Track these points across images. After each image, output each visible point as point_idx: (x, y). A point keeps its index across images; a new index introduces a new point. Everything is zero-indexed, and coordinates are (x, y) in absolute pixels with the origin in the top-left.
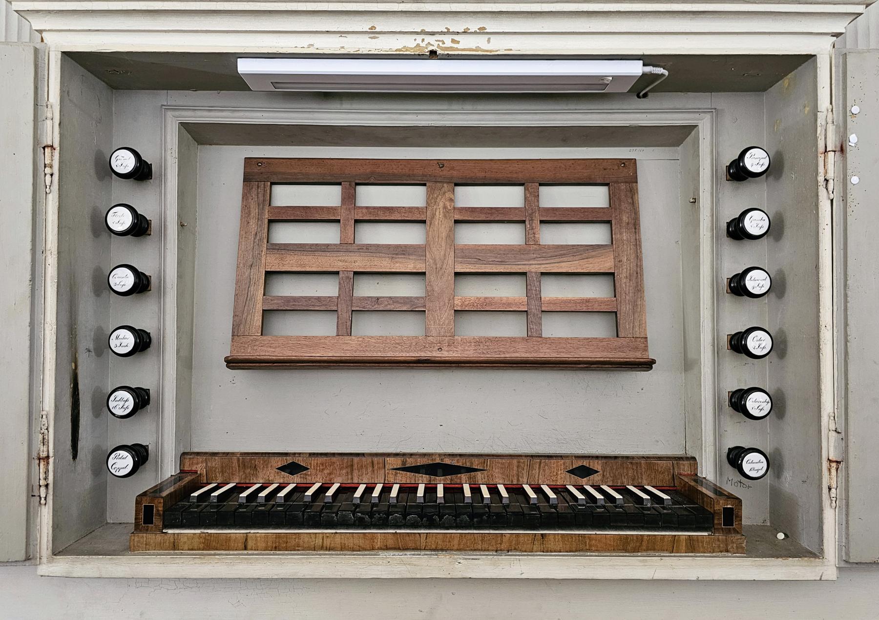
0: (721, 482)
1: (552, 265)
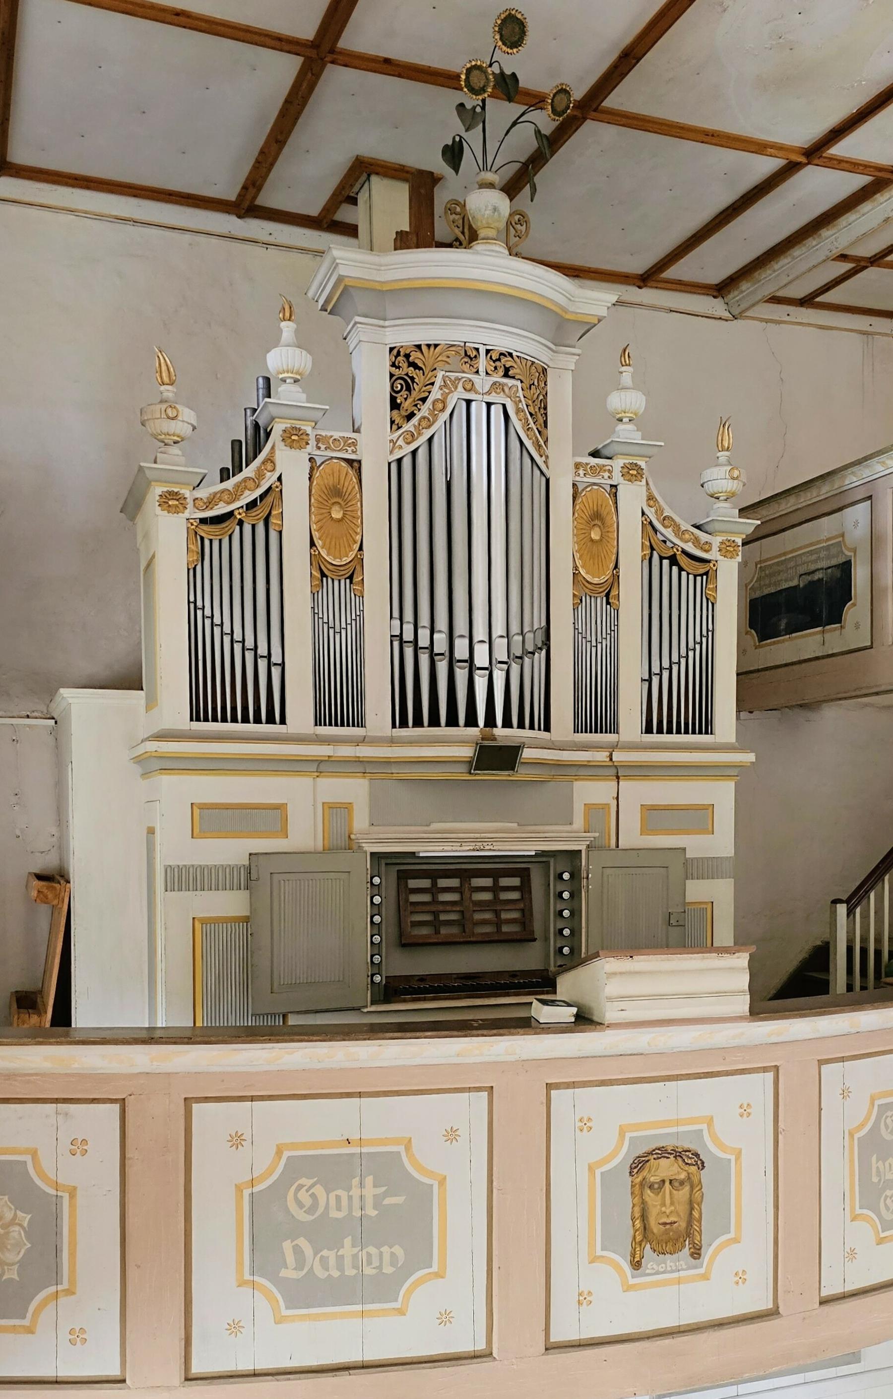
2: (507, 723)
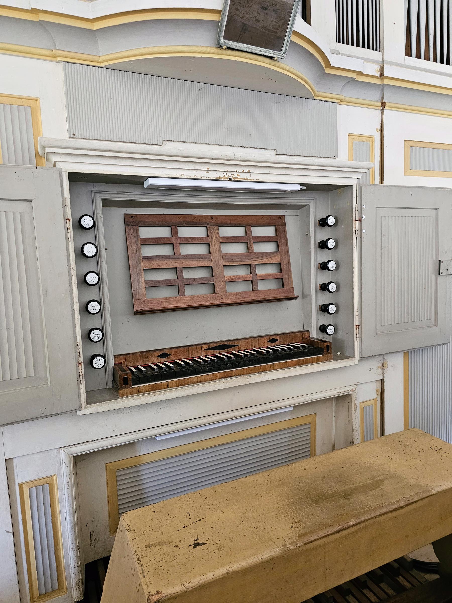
0: (318, 337)
1: (259, 261)
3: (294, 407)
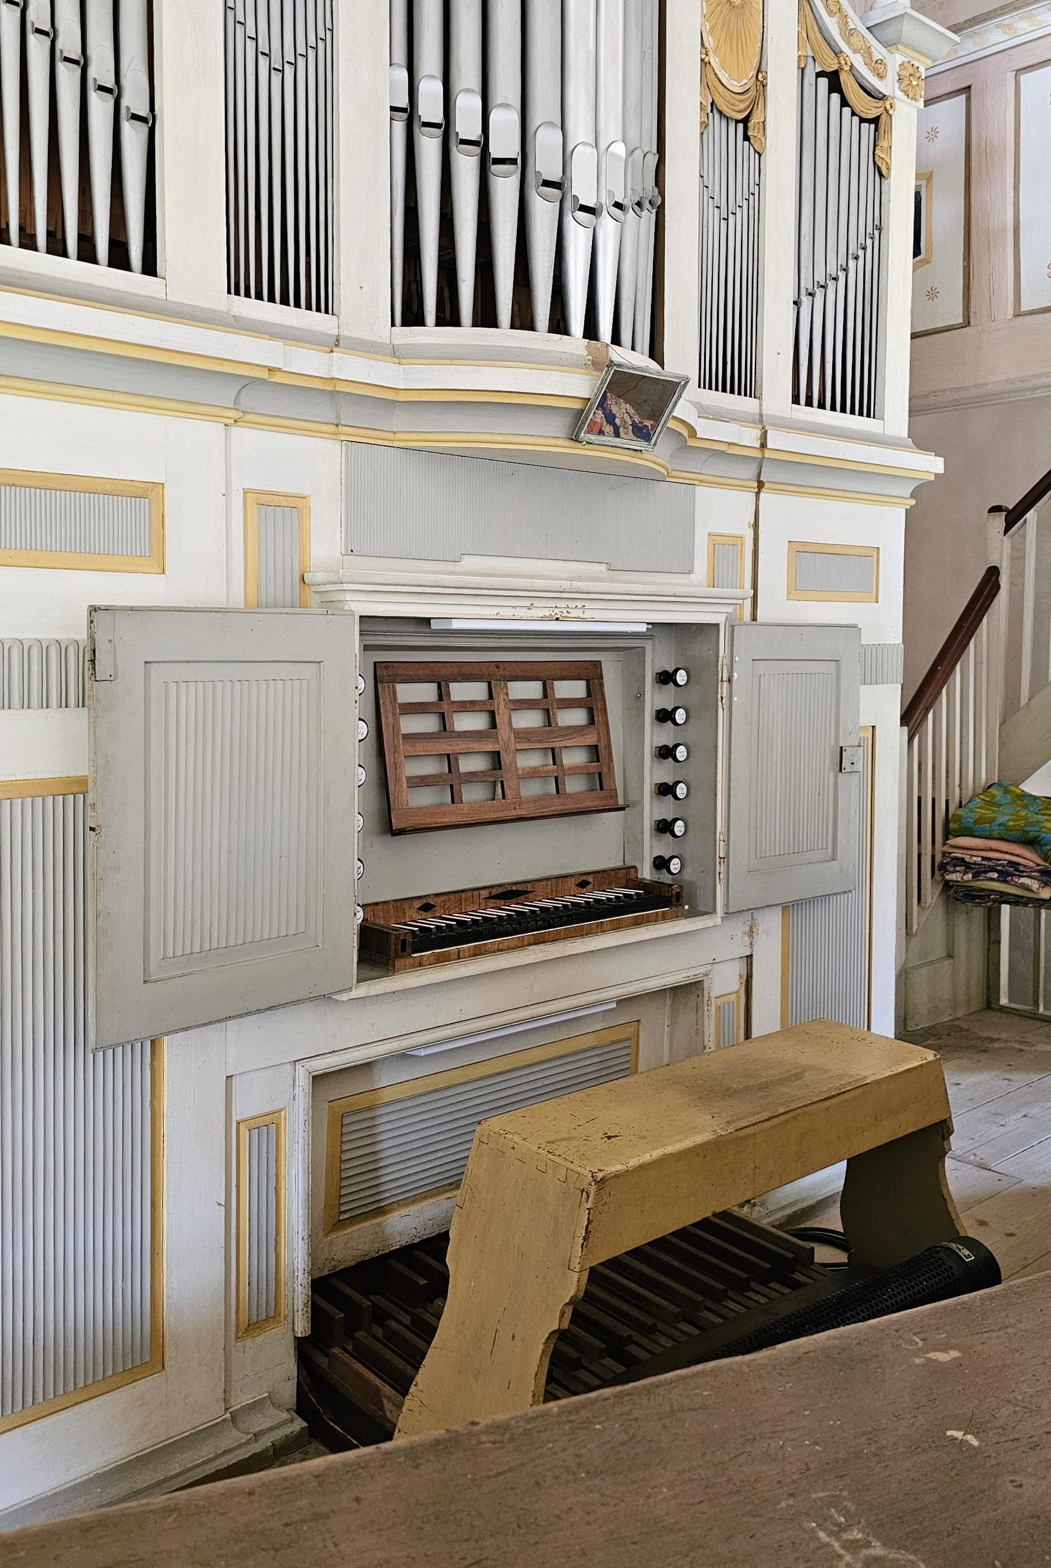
2: (616, 340)
3: (618, 1002)
